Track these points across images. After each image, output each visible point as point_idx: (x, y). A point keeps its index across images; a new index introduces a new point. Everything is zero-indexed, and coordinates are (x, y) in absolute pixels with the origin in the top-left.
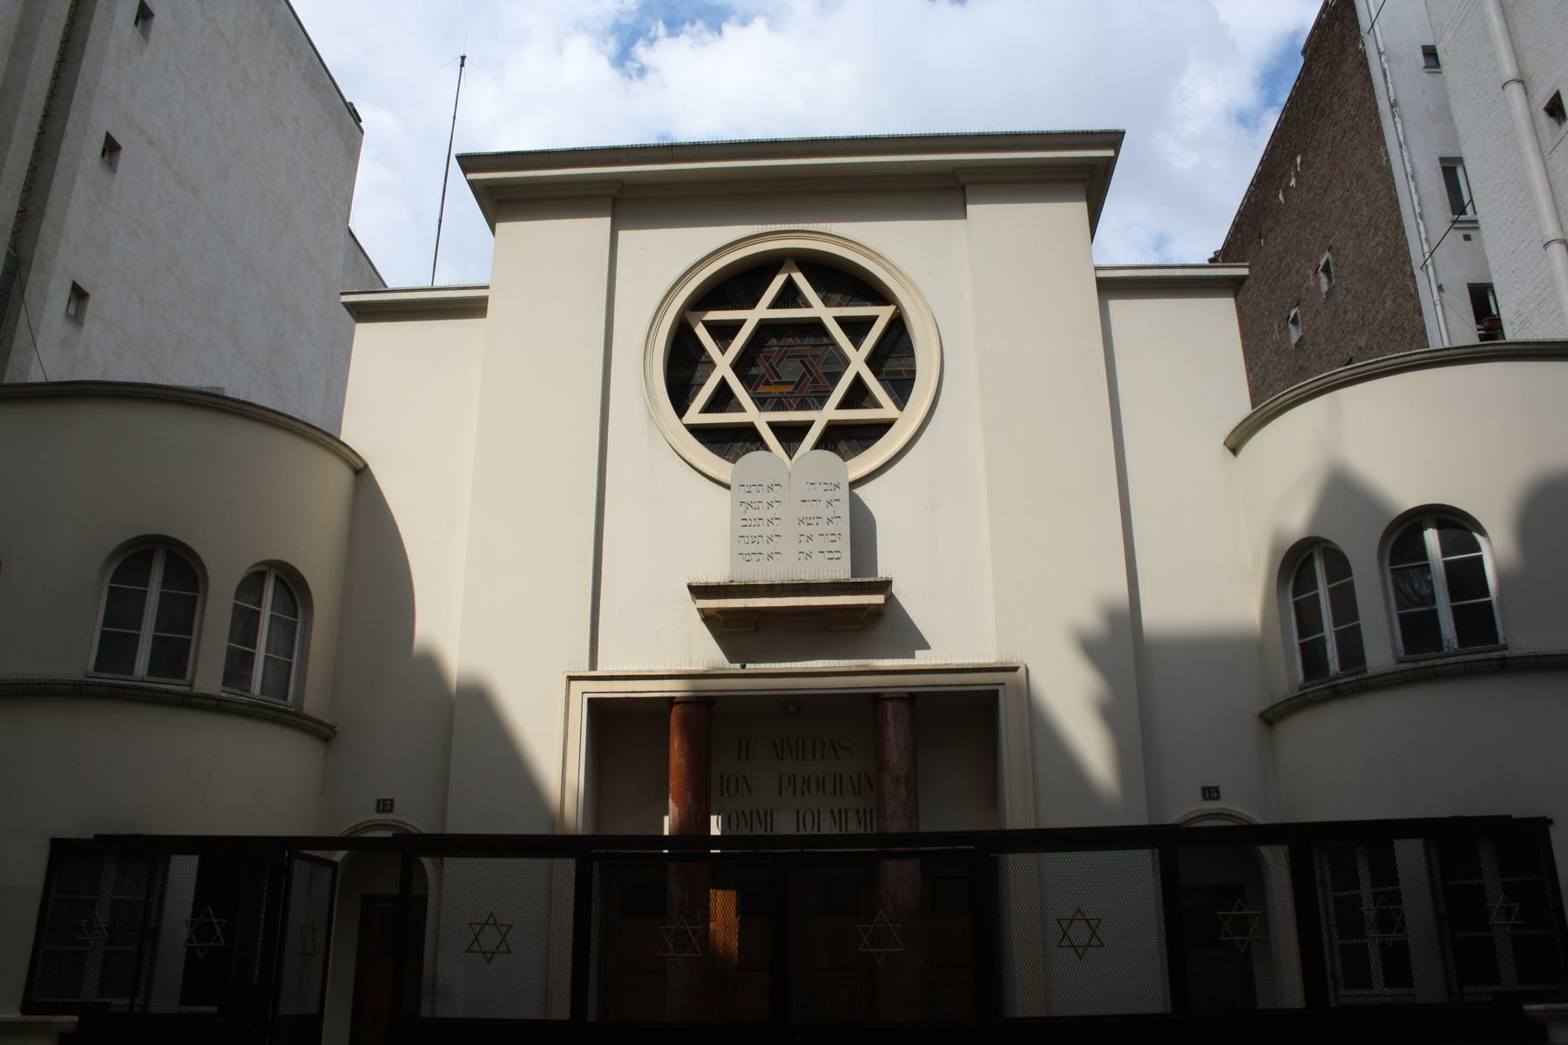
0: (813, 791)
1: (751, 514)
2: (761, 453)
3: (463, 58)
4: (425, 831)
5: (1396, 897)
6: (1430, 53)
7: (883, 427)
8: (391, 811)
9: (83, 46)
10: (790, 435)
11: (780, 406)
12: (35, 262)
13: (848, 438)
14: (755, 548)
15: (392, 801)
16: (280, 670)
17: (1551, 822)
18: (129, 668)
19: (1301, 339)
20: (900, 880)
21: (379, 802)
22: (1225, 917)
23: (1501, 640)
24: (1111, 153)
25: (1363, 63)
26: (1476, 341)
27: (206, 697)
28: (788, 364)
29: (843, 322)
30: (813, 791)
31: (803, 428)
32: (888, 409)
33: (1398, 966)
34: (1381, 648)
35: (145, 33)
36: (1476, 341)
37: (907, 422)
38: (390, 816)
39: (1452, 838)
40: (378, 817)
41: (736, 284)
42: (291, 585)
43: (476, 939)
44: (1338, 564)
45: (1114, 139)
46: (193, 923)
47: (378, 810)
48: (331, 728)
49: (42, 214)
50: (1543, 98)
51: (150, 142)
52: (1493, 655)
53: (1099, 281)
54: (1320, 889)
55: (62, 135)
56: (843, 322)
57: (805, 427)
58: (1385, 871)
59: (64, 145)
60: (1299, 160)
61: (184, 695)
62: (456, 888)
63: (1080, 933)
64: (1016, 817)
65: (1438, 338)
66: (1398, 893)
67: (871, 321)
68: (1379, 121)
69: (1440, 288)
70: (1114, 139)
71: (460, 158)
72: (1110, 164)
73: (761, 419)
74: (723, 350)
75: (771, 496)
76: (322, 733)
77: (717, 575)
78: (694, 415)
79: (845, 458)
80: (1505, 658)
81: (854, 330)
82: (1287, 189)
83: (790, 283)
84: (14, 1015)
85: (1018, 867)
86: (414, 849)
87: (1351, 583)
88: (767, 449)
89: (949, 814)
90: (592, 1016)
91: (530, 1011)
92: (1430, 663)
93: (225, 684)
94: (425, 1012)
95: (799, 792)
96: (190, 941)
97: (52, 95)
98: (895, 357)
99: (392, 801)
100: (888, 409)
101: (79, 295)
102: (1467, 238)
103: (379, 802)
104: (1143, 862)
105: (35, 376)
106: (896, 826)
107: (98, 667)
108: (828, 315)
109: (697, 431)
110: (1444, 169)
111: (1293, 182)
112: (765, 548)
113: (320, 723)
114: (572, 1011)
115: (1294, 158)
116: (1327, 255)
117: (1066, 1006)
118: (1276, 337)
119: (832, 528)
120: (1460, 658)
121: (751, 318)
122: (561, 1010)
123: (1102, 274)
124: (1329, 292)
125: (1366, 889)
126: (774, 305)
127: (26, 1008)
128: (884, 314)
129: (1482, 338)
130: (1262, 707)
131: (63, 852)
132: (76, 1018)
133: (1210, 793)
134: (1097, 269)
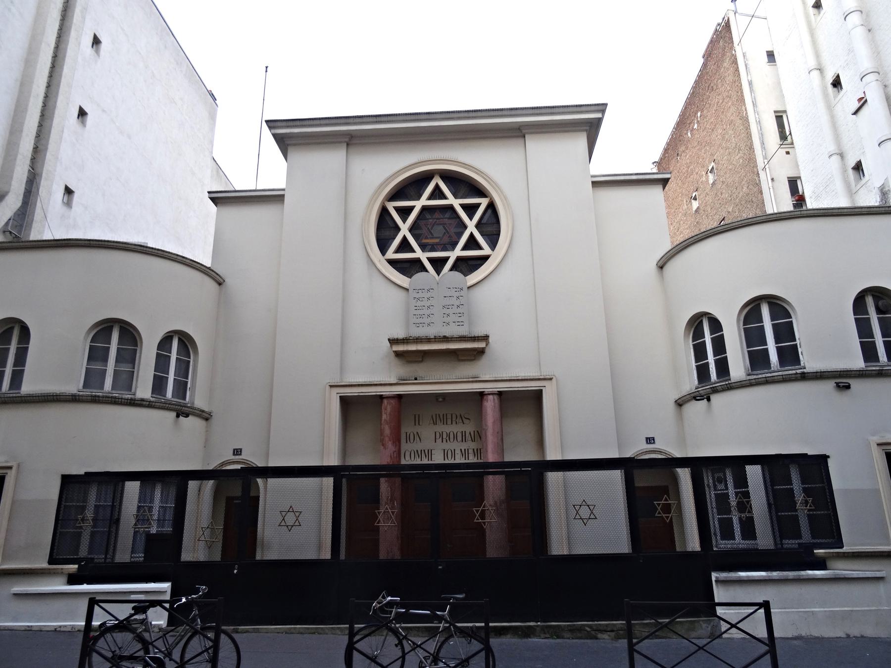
0: (452, 440)
1: (419, 303)
2: (424, 273)
4: (259, 465)
5: (747, 495)
6: (771, 56)
7: (485, 258)
9: (64, 59)
10: (438, 264)
11: (433, 249)
12: (44, 175)
13: (467, 265)
14: (421, 320)
15: (241, 450)
16: (181, 388)
17: (828, 457)
18: (102, 386)
19: (698, 208)
20: (494, 485)
22: (659, 505)
23: (802, 364)
24: (599, 115)
25: (735, 62)
26: (792, 209)
27: (142, 400)
28: (438, 227)
29: (464, 207)
30: (452, 440)
32: (486, 250)
33: (749, 530)
34: (738, 368)
35: (97, 52)
36: (792, 209)
38: (240, 457)
39: (774, 465)
40: (233, 457)
41: (412, 186)
42: (186, 342)
44: (716, 325)
45: (602, 108)
46: (137, 516)
47: (234, 454)
48: (210, 414)
49: (46, 149)
50: (830, 79)
51: (104, 111)
52: (798, 371)
53: (594, 183)
54: (707, 489)
55: (55, 107)
56: (464, 207)
57: (446, 259)
58: (741, 481)
59: (57, 112)
60: (699, 114)
61: (131, 399)
62: (271, 492)
63: (585, 512)
64: (552, 455)
65: (771, 208)
66: (748, 492)
67: (477, 206)
68: (742, 92)
69: (772, 179)
70: (602, 108)
71: (267, 122)
74: (404, 221)
76: (205, 416)
77: (401, 335)
78: (391, 254)
79: (465, 275)
80: (803, 373)
81: (470, 210)
82: (693, 129)
83: (437, 187)
84: (45, 565)
85: (553, 478)
86: (253, 473)
87: (722, 335)
88: (427, 271)
89: (520, 452)
90: (343, 556)
91: (310, 554)
92: (764, 376)
93: (865, 361)
94: (258, 557)
96: (135, 525)
97: (49, 86)
98: (491, 226)
99: (241, 450)
100: (486, 250)
101: (69, 191)
102: (788, 153)
104: (617, 475)
105: (47, 236)
106: (491, 458)
107: (85, 386)
108: (456, 203)
109: (392, 262)
110: (776, 117)
111: (696, 126)
113: (203, 411)
115: (696, 113)
116: (713, 164)
117: (581, 549)
118: (685, 207)
120: (780, 373)
121: (418, 205)
124: (714, 184)
125: (731, 491)
126: (429, 198)
127: (50, 563)
128: (484, 202)
129: (795, 206)
130: (677, 398)
131: (66, 480)
132: (76, 566)
133: (650, 440)
134: (592, 176)
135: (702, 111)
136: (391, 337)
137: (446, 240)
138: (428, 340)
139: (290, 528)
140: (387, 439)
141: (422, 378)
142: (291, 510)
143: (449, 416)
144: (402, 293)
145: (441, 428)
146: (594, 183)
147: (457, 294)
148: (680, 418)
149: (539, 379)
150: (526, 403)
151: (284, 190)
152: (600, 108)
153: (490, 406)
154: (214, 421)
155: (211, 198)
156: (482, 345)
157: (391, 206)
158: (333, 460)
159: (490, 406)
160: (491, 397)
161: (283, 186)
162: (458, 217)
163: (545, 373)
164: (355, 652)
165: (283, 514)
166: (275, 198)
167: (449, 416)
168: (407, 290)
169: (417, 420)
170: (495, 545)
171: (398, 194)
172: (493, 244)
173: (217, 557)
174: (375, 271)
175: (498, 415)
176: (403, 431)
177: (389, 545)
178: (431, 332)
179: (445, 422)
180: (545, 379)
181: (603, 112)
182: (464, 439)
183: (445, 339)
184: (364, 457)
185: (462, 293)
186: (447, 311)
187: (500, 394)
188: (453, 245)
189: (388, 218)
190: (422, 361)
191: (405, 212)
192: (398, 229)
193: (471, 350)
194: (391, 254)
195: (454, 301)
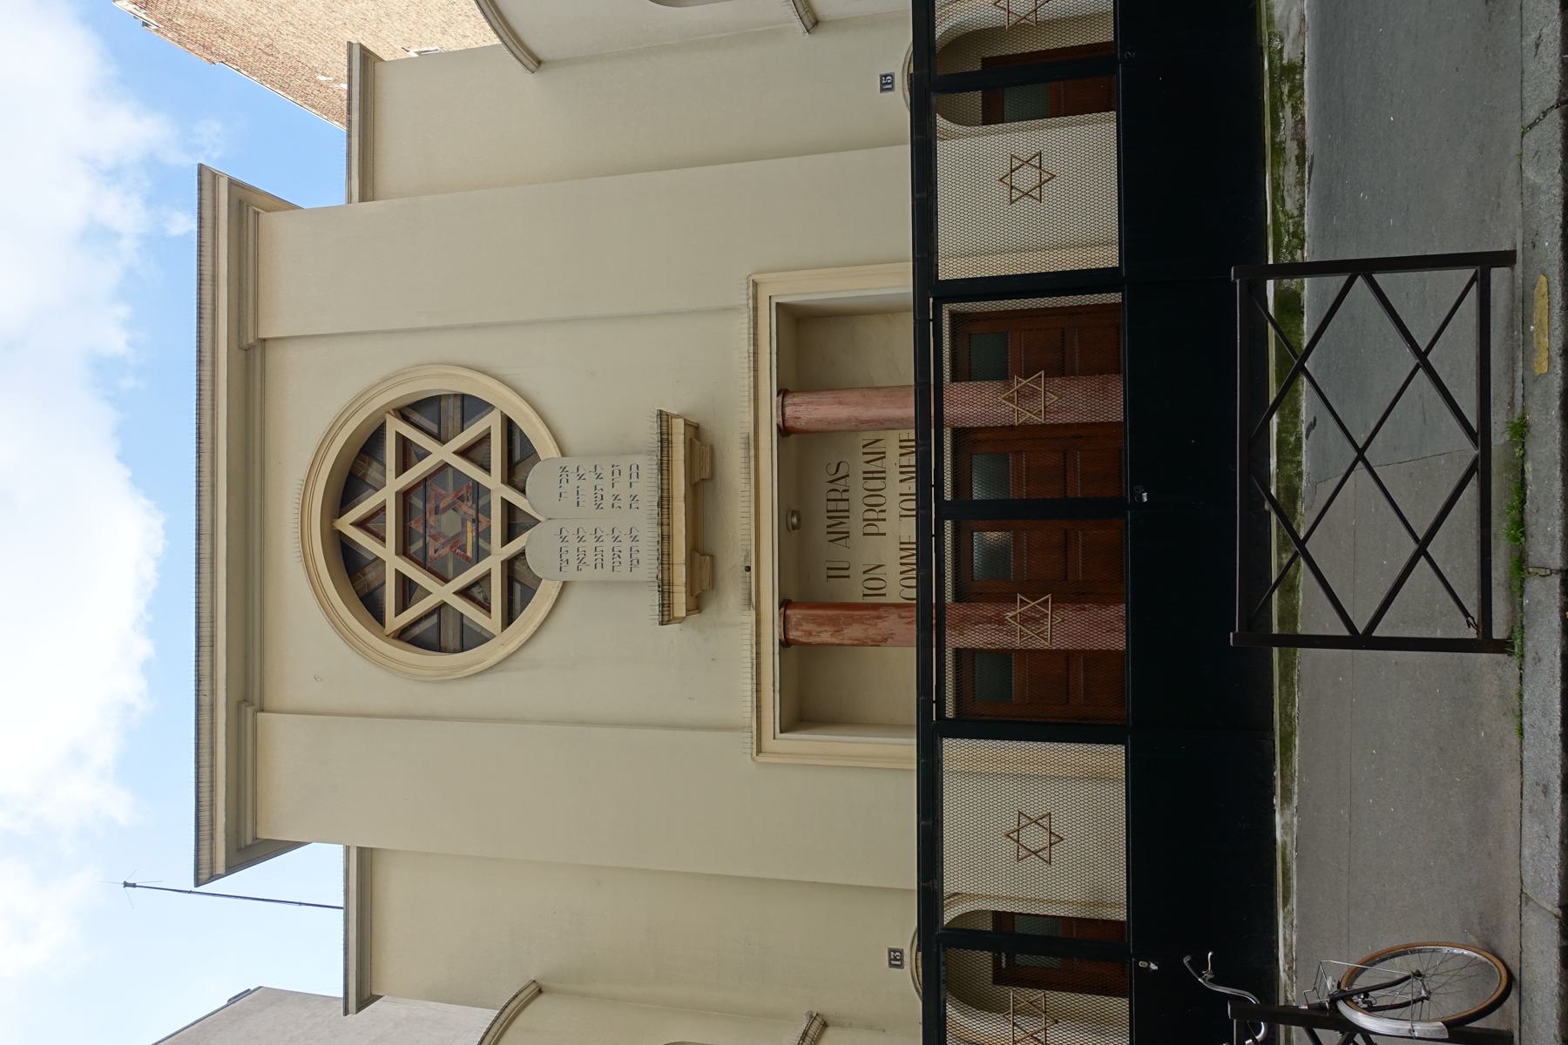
0: (881, 500)
1: (590, 559)
3: (126, 885)
7: (509, 425)
8: (901, 952)
10: (514, 523)
11: (486, 534)
13: (518, 457)
14: (625, 555)
20: (971, 404)
21: (891, 965)
29: (403, 466)
30: (881, 500)
31: (509, 509)
32: (491, 423)
37: (507, 402)
38: (907, 952)
40: (907, 967)
43: (1035, 853)
48: (813, 1018)
53: (362, 199)
62: (981, 882)
71: (197, 884)
72: (232, 183)
73: (499, 553)
75: (572, 538)
83: (361, 524)
91: (1115, 799)
94: (1121, 914)
95: (882, 516)
100: (491, 423)
103: (891, 965)
109: (509, 618)
112: (625, 545)
113: (805, 1034)
114: (1115, 743)
119: (607, 474)
122: (1113, 758)
123: (356, 196)
128: (395, 426)
132: (1276, 650)
134: (350, 200)
135: (314, 70)
136: (657, 618)
137: (468, 508)
138: (665, 539)
139: (1055, 839)
140: (872, 632)
141: (747, 556)
142: (1014, 835)
143: (832, 506)
144: (573, 598)
145: (855, 525)
146: (362, 199)
147: (573, 478)
148: (844, 24)
149: (755, 309)
150: (807, 339)
151: (347, 849)
152: (207, 179)
153: (809, 411)
154: (826, 1007)
155: (359, 1009)
156: (678, 428)
157: (394, 622)
158: (906, 748)
159: (809, 411)
160: (788, 411)
161: (340, 849)
162: (424, 482)
163: (742, 298)
164: (1343, 279)
165: (1025, 853)
166: (364, 871)
167: (832, 506)
168: (565, 583)
169: (839, 572)
170: (1097, 402)
171: (371, 605)
172: (482, 407)
173: (1119, 1007)
174: (530, 652)
175: (828, 397)
176: (860, 600)
177: (1101, 629)
178: (648, 535)
179: (844, 515)
180: (755, 298)
181: (215, 176)
182: (880, 475)
183: (664, 502)
184: (893, 671)
185: (571, 468)
186: (608, 499)
187: (783, 392)
188: (478, 491)
189: (417, 631)
190: (712, 556)
191: (408, 591)
192: (441, 607)
193: (692, 456)
194: (492, 622)
195: (587, 486)
